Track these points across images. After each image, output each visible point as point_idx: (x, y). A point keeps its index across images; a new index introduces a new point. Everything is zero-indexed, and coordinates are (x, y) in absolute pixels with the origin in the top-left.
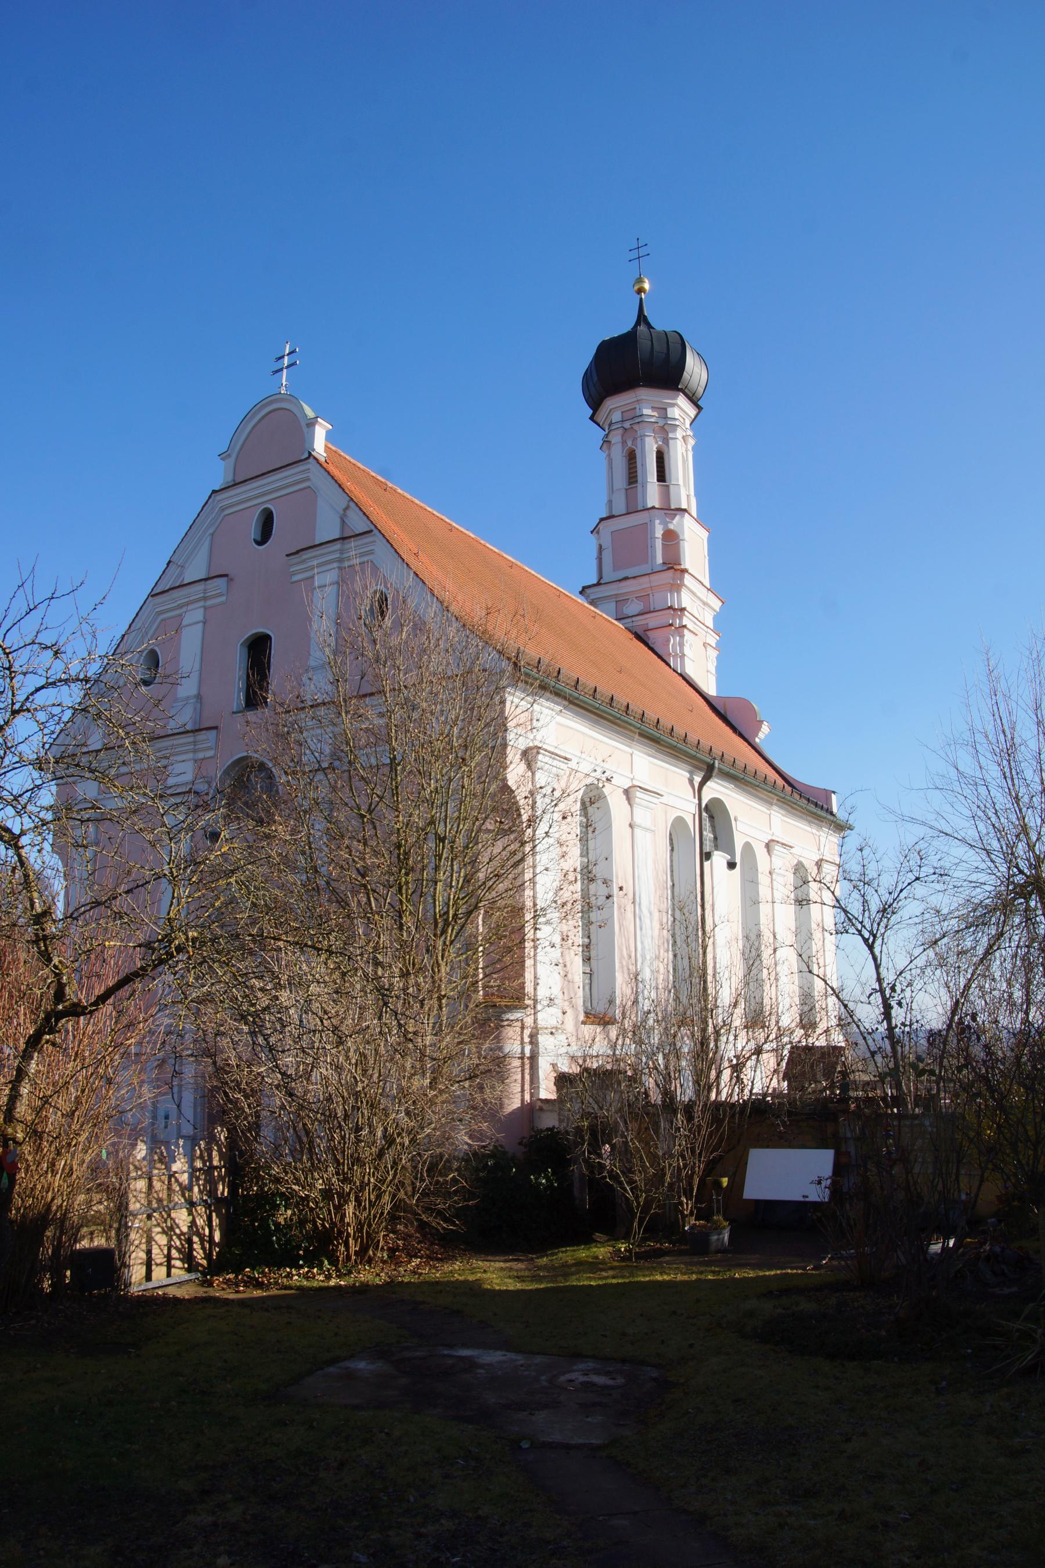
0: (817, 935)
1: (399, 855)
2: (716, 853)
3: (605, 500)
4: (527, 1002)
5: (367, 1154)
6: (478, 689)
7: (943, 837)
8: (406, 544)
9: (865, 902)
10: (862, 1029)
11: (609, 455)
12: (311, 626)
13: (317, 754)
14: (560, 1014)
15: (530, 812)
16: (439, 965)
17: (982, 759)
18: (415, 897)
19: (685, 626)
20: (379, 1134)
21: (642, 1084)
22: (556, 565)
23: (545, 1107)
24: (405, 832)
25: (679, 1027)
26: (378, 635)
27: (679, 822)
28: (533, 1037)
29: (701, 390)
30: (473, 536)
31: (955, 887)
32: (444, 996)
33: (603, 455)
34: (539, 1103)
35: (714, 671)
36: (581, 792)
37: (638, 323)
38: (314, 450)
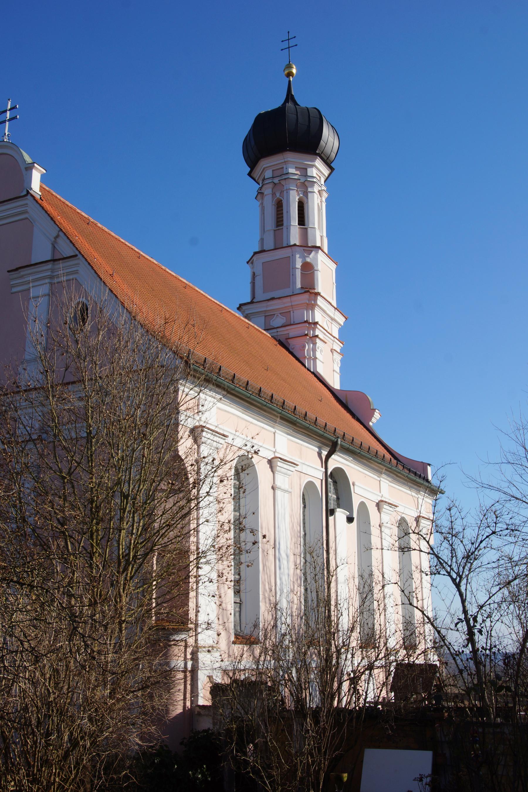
0: (416, 575)
1: (91, 508)
2: (338, 510)
3: (258, 238)
4: (191, 626)
5: (55, 756)
6: (157, 381)
8: (104, 266)
9: (453, 550)
10: (452, 650)
11: (262, 204)
12: (26, 328)
13: (28, 429)
14: (216, 636)
15: (195, 476)
16: (121, 596)
18: (104, 542)
19: (317, 336)
20: (66, 738)
21: (280, 693)
22: (221, 289)
23: (202, 712)
24: (97, 490)
25: (309, 648)
26: (80, 336)
27: (310, 485)
28: (195, 658)
29: (333, 155)
30: (156, 263)
31: (524, 540)
32: (124, 621)
34: (198, 709)
35: (338, 371)
36: (235, 462)
37: (286, 101)
38: (31, 189)
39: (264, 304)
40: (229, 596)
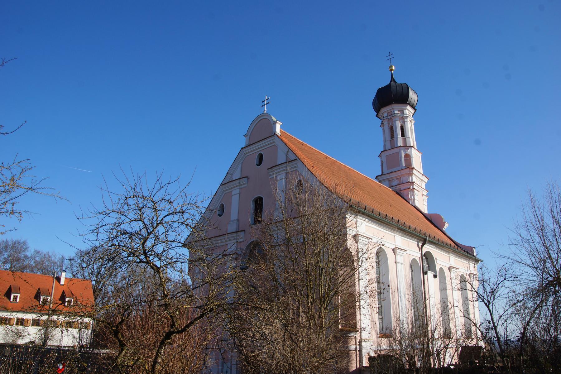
7: (518, 264)
9: (484, 289)
17: (531, 233)
22: (367, 168)
23: (365, 369)
27: (414, 261)
28: (360, 344)
29: (415, 103)
33: (381, 129)
37: (391, 81)
39: (388, 175)
40: (376, 317)
